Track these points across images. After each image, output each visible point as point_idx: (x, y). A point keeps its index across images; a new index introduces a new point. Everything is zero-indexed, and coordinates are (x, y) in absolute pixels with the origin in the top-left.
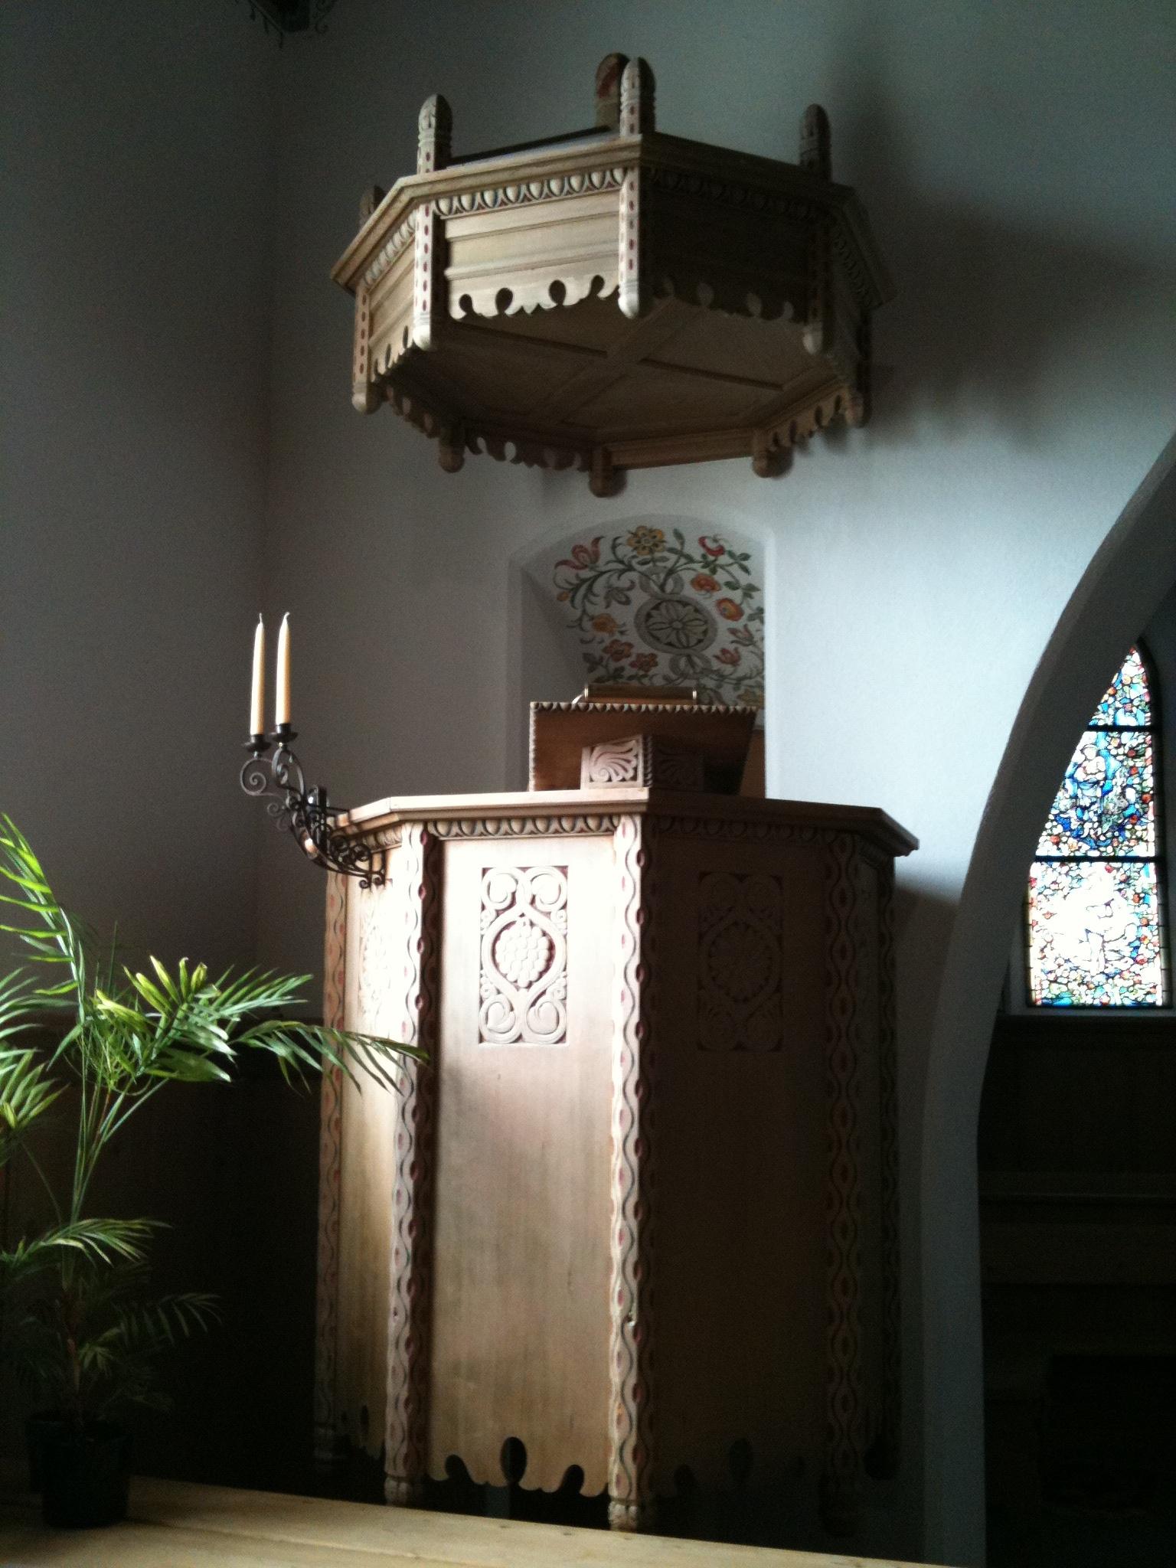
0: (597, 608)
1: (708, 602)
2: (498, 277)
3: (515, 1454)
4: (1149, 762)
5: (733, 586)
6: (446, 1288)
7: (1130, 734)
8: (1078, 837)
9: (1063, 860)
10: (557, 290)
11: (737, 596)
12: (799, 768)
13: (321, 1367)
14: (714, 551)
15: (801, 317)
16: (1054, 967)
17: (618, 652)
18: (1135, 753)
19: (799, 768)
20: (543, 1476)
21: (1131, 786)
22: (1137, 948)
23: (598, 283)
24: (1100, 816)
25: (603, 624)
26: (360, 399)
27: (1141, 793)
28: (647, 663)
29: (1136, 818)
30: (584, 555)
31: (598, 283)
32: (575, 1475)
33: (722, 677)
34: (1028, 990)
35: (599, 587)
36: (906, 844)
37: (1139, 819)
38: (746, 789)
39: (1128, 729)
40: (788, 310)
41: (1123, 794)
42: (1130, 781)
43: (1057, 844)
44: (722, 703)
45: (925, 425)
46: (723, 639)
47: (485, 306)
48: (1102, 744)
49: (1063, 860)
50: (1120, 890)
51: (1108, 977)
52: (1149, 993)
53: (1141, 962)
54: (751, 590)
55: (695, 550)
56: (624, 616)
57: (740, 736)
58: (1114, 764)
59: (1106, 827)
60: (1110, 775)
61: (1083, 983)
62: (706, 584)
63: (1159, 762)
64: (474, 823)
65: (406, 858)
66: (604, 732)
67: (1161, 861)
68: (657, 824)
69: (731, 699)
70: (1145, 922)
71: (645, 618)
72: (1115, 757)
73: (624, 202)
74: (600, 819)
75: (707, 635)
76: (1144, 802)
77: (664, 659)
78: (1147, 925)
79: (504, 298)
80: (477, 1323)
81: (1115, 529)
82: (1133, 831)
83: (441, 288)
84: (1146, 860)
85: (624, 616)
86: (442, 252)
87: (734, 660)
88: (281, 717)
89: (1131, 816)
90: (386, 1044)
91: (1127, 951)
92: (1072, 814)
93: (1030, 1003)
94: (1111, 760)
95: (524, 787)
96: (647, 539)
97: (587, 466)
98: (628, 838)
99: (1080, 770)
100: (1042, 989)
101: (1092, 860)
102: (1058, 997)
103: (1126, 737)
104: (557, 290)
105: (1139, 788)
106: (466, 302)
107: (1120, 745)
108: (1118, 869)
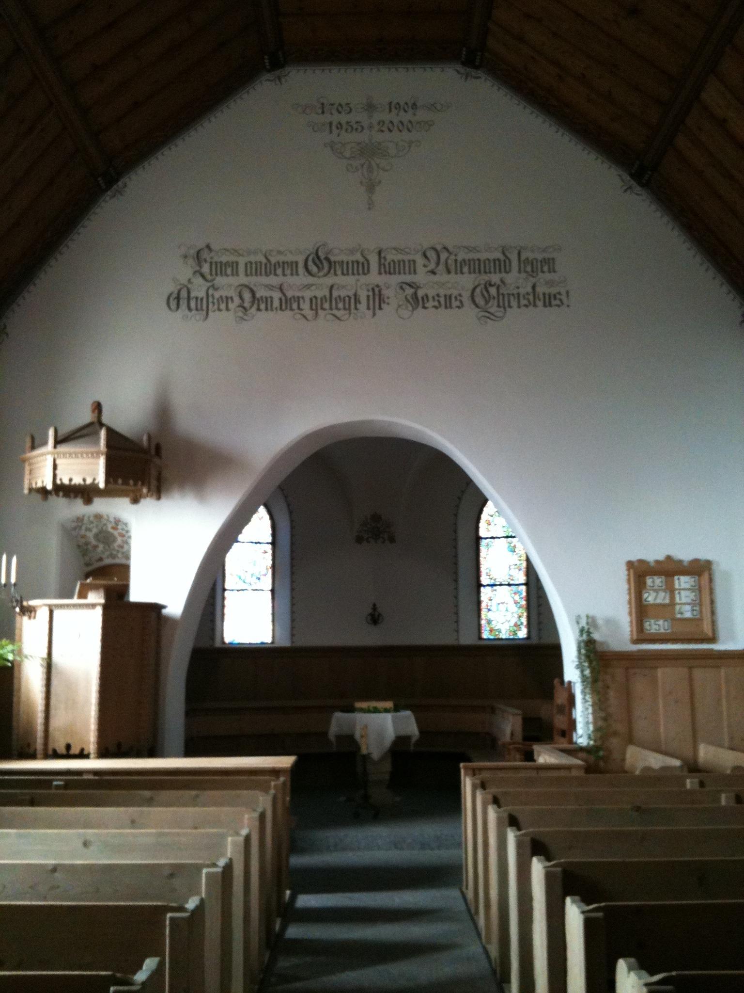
0: (83, 532)
1: (115, 533)
2: (218, 909)
3: (68, 747)
5: (123, 529)
6: (52, 712)
10: (84, 480)
11: (124, 532)
12: (137, 595)
13: (14, 737)
14: (117, 521)
15: (143, 484)
17: (87, 544)
19: (137, 595)
20: (75, 750)
23: (94, 480)
25: (83, 537)
26: (26, 491)
28: (96, 547)
30: (80, 520)
31: (94, 480)
32: (82, 750)
33: (118, 551)
34: (223, 638)
35: (84, 528)
36: (164, 607)
38: (125, 599)
40: (140, 483)
45: (176, 495)
46: (119, 540)
47: (66, 481)
54: (127, 532)
55: (111, 519)
56: (90, 535)
57: (124, 590)
62: (115, 528)
64: (61, 606)
65: (43, 614)
66: (95, 587)
68: (106, 608)
69: (123, 561)
71: (96, 536)
73: (102, 461)
74: (93, 606)
75: (114, 540)
77: (101, 547)
79: (71, 480)
80: (59, 720)
81: (231, 513)
83: (55, 476)
85: (90, 535)
86: (55, 467)
87: (122, 547)
88: (13, 580)
93: (224, 643)
95: (71, 596)
96: (98, 517)
97: (82, 497)
98: (99, 611)
100: (227, 640)
104: (84, 480)
106: (61, 480)
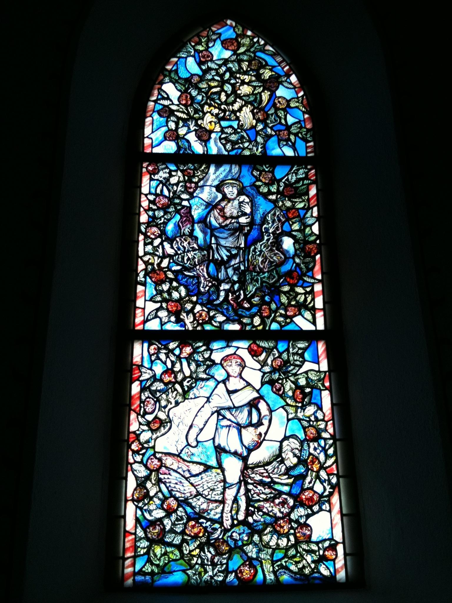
4: (313, 202)
7: (286, 169)
8: (209, 304)
9: (184, 338)
16: (159, 514)
18: (293, 191)
21: (289, 234)
22: (302, 477)
24: (242, 275)
27: (302, 244)
29: (296, 277)
37: (301, 277)
39: (283, 160)
41: (277, 244)
42: (286, 227)
43: (177, 314)
44: (182, 127)
48: (247, 181)
49: (184, 338)
50: (272, 382)
51: (254, 530)
52: (323, 559)
53: (308, 504)
58: (263, 206)
59: (251, 289)
60: (258, 218)
61: (208, 543)
63: (325, 201)
67: (333, 336)
70: (312, 431)
72: (265, 196)
76: (308, 254)
78: (316, 439)
82: (292, 294)
84: (311, 337)
89: (289, 274)
90: (231, 56)
91: (284, 484)
92: (202, 270)
94: (260, 200)
99: (216, 212)
101: (229, 337)
102: (164, 571)
103: (280, 172)
105: (299, 235)
107: (273, 181)
108: (269, 351)
